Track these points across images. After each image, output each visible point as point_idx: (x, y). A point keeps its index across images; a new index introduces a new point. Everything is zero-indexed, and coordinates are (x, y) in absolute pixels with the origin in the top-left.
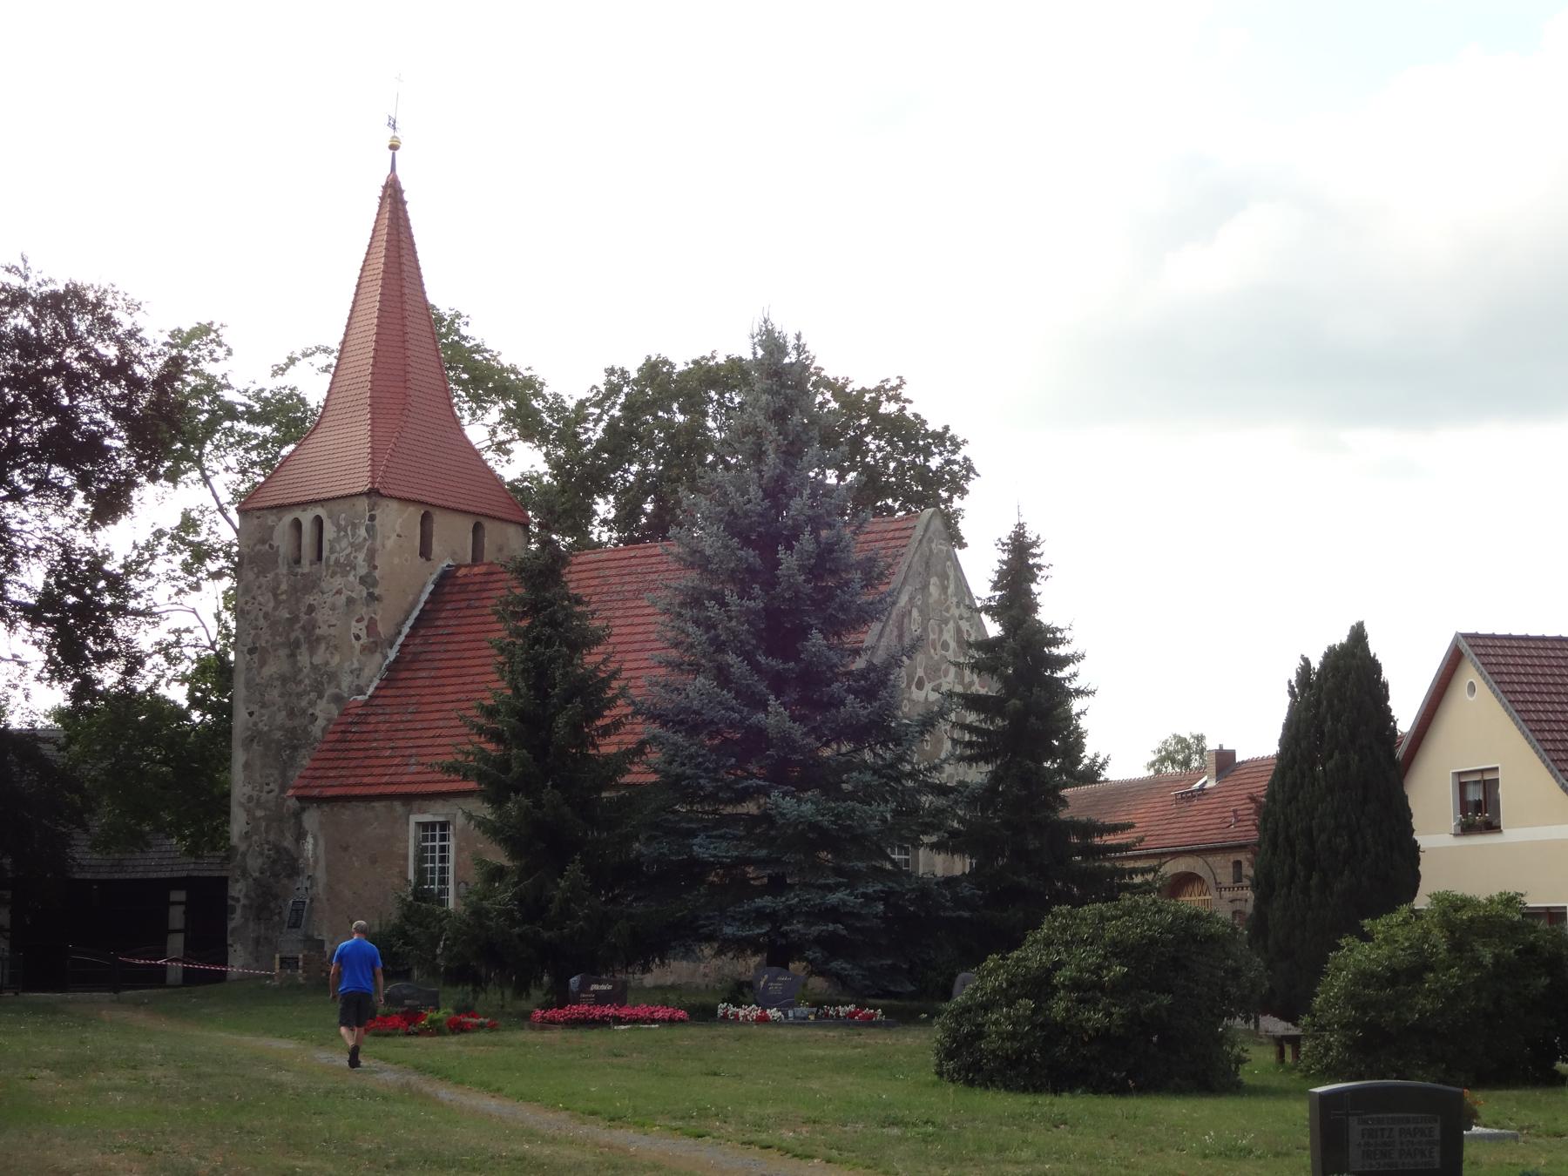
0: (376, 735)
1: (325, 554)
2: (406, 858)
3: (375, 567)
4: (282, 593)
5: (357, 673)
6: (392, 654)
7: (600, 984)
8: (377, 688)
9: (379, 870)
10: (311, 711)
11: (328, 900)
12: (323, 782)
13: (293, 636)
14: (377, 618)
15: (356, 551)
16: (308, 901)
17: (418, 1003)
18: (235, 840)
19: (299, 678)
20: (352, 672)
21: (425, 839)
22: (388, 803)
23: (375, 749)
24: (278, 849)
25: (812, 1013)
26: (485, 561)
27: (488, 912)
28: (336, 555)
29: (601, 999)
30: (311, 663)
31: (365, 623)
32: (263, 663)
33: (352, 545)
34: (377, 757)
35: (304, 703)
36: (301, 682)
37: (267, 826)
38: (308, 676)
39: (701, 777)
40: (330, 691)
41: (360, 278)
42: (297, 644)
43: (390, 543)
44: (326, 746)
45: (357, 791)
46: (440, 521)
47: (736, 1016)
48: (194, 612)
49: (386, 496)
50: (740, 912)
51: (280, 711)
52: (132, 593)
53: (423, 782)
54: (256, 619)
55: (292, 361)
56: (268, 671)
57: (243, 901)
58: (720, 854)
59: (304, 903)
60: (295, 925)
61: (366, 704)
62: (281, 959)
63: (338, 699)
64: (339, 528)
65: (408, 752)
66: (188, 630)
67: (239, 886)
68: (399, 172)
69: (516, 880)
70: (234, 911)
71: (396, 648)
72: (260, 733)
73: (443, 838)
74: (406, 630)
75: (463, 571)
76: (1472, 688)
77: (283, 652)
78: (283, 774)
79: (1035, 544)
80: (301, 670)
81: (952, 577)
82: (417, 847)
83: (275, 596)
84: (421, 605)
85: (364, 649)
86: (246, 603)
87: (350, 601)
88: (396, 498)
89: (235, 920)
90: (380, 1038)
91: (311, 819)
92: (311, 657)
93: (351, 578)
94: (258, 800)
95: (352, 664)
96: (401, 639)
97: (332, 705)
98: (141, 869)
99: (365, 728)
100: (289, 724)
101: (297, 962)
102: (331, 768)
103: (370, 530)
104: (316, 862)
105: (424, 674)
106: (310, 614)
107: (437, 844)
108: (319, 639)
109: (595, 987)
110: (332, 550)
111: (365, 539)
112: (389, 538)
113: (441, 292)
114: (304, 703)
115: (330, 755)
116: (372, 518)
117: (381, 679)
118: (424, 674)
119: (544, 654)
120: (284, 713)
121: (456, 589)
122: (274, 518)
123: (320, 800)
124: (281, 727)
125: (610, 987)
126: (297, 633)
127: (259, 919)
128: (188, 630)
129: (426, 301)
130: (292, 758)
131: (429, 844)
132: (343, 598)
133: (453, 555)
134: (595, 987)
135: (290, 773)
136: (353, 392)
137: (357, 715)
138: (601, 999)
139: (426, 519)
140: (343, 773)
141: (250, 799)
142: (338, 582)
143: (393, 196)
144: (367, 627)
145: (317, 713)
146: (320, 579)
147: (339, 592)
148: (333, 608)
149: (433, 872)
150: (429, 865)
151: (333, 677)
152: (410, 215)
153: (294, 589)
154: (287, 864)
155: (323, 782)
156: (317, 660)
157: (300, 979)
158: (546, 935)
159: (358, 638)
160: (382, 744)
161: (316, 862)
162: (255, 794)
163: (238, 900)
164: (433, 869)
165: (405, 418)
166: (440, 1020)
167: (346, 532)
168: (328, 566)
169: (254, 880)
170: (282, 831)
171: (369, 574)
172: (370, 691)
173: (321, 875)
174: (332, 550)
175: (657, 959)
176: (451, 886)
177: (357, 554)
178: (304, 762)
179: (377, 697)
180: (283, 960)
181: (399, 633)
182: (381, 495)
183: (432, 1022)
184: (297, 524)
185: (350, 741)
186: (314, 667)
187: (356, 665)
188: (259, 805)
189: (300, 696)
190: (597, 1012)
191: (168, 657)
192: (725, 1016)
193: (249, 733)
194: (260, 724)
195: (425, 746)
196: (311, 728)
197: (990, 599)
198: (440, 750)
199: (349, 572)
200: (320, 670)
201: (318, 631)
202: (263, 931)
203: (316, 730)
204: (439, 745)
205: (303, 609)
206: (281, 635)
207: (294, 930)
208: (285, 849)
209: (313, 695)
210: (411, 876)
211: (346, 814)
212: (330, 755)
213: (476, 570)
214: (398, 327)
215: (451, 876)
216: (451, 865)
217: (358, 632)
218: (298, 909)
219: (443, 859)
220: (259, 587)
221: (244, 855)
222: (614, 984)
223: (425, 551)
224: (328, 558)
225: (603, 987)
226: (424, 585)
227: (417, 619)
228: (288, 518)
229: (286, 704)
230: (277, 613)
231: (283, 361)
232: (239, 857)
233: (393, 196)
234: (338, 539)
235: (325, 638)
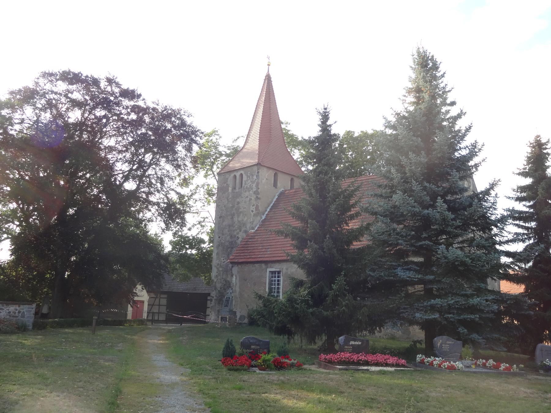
0: (257, 242)
1: (243, 185)
2: (266, 284)
3: (259, 188)
4: (230, 199)
5: (252, 223)
6: (264, 217)
7: (355, 341)
8: (258, 228)
9: (256, 288)
11: (239, 298)
14: (259, 205)
17: (258, 347)
18: (213, 278)
19: (234, 225)
21: (272, 277)
22: (260, 264)
23: (257, 246)
24: (226, 281)
25: (473, 364)
26: (295, 188)
27: (296, 300)
29: (356, 350)
30: (238, 220)
31: (255, 206)
33: (251, 182)
34: (257, 249)
35: (235, 233)
36: (235, 226)
39: (399, 240)
40: (243, 229)
41: (257, 103)
42: (234, 215)
43: (264, 181)
44: (241, 246)
45: (250, 260)
46: (280, 176)
47: (431, 364)
48: (208, 212)
49: (263, 166)
50: (421, 307)
51: (228, 236)
52: (186, 198)
53: (272, 257)
54: (222, 207)
55: (238, 138)
56: (224, 224)
57: (215, 298)
58: (412, 277)
59: (230, 298)
60: (226, 306)
61: (254, 233)
62: (221, 317)
63: (246, 232)
64: (248, 176)
65: (267, 247)
66: (207, 218)
68: (270, 72)
69: (309, 285)
71: (265, 215)
72: (222, 243)
73: (279, 277)
74: (268, 210)
75: (287, 192)
77: (229, 217)
79: (545, 144)
80: (235, 223)
81: (471, 183)
82: (269, 280)
83: (228, 200)
84: (273, 203)
85: (254, 215)
86: (219, 202)
88: (266, 167)
90: (231, 372)
91: (235, 270)
92: (238, 218)
93: (251, 192)
94: (220, 265)
96: (266, 213)
97: (244, 234)
98: (200, 290)
99: (253, 240)
100: (231, 240)
101: (226, 319)
102: (242, 253)
103: (258, 176)
104: (236, 284)
105: (273, 223)
107: (276, 279)
109: (352, 343)
110: (245, 184)
111: (256, 179)
112: (263, 179)
113: (283, 116)
115: (243, 249)
116: (258, 172)
117: (260, 225)
118: (273, 223)
119: (324, 178)
120: (229, 237)
121: (285, 197)
125: (360, 343)
128: (207, 218)
129: (280, 120)
130: (231, 251)
131: (274, 279)
134: (352, 343)
136: (254, 137)
137: (252, 236)
138: (356, 350)
139: (276, 175)
140: (246, 254)
141: (218, 264)
142: (247, 194)
143: (268, 79)
144: (255, 208)
145: (239, 236)
147: (247, 197)
149: (275, 289)
150: (273, 286)
151: (244, 224)
152: (273, 85)
154: (227, 285)
156: (240, 219)
157: (227, 325)
158: (325, 313)
159: (252, 211)
160: (258, 245)
161: (236, 284)
162: (219, 263)
163: (213, 297)
164: (275, 288)
165: (269, 145)
166: (269, 360)
167: (250, 178)
168: (244, 189)
171: (257, 191)
173: (238, 289)
174: (245, 184)
175: (378, 328)
176: (281, 294)
179: (258, 230)
180: (222, 318)
181: (266, 211)
182: (261, 165)
183: (264, 361)
185: (249, 244)
186: (239, 221)
187: (252, 221)
189: (234, 231)
190: (355, 357)
191: (202, 226)
192: (422, 362)
194: (222, 241)
195: (273, 245)
197: (524, 169)
198: (278, 246)
199: (250, 190)
201: (240, 210)
203: (239, 242)
204: (278, 245)
207: (226, 307)
208: (228, 281)
209: (238, 231)
210: (267, 290)
211: (247, 268)
212: (243, 249)
213: (291, 191)
215: (281, 290)
216: (281, 287)
217: (253, 210)
218: (228, 300)
219: (278, 284)
221: (215, 283)
222: (362, 341)
223: (275, 185)
224: (244, 186)
225: (357, 343)
226: (274, 196)
227: (272, 206)
228: (232, 175)
229: (229, 234)
231: (238, 139)
233: (268, 79)
234: (247, 180)
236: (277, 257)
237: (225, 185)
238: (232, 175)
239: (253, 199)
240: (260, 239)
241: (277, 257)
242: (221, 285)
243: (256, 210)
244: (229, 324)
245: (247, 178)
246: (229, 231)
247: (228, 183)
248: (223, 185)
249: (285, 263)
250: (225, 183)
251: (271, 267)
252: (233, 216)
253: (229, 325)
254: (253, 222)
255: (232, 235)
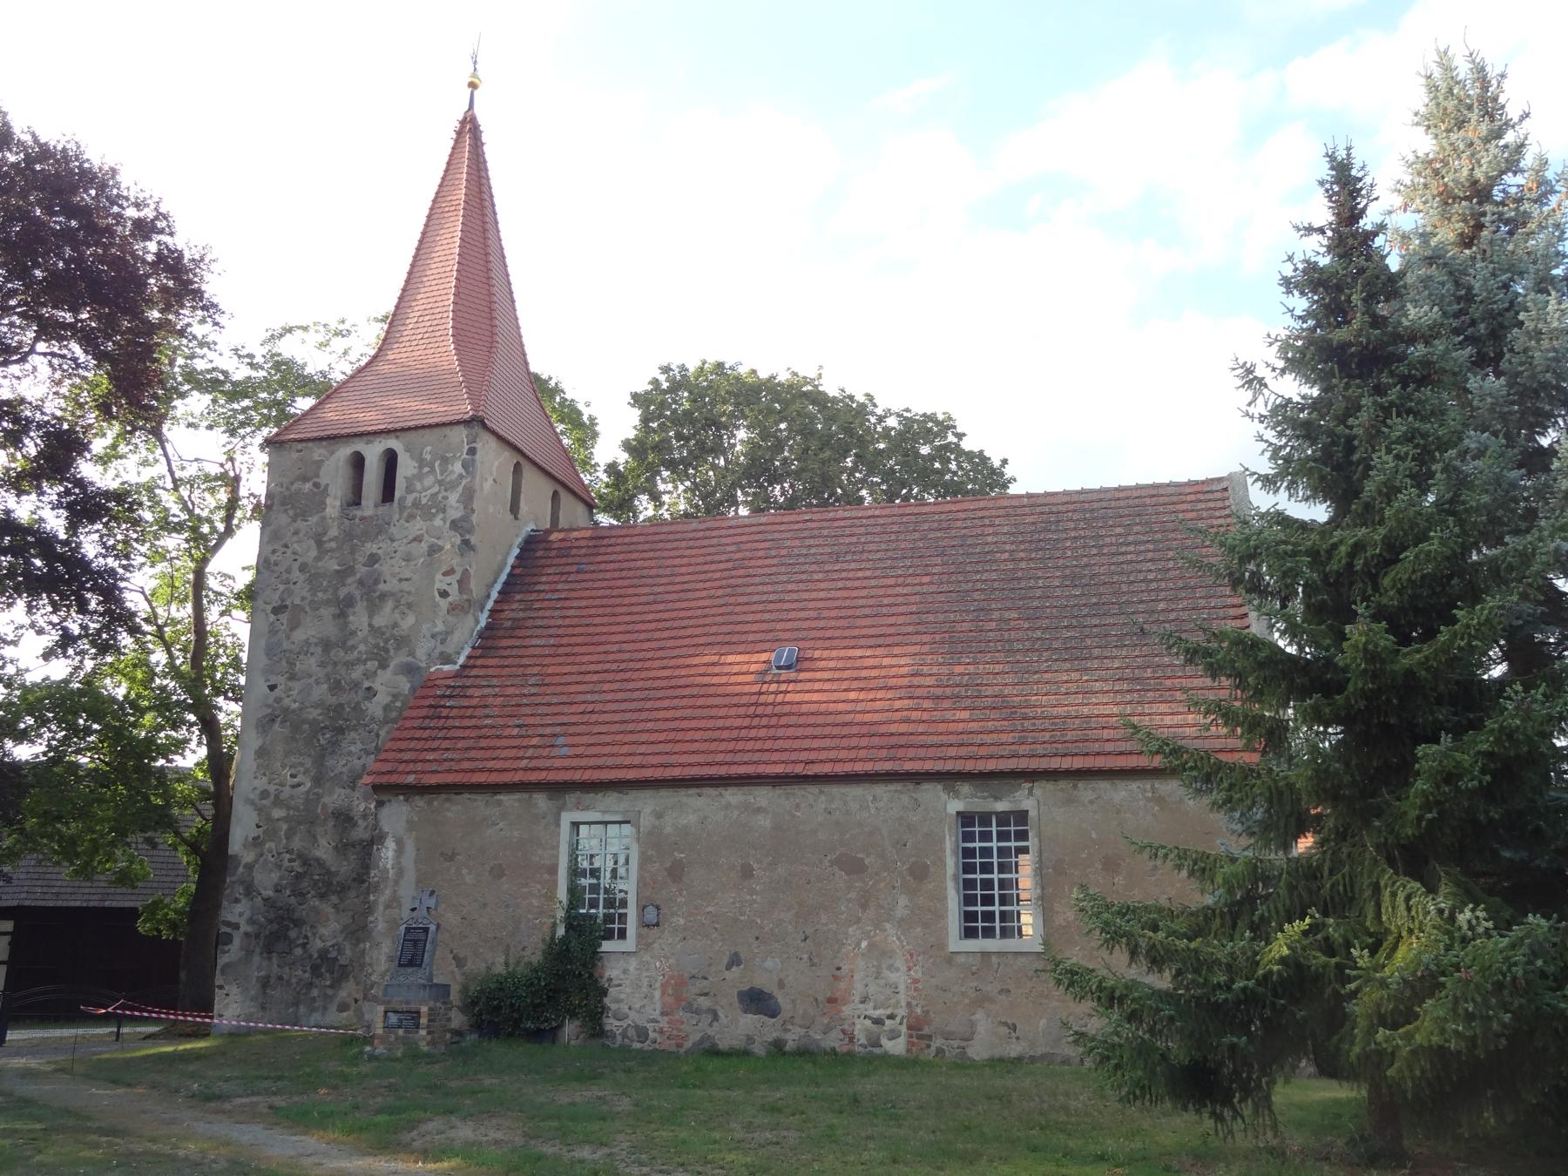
0: (487, 711)
1: (398, 494)
2: (553, 870)
4: (331, 540)
5: (443, 637)
10: (366, 684)
12: (419, 767)
13: (343, 593)
15: (446, 490)
16: (432, 928)
19: (350, 643)
20: (433, 636)
22: (526, 796)
28: (415, 495)
30: (370, 625)
31: (457, 576)
32: (294, 625)
33: (440, 483)
37: (290, 829)
38: (365, 641)
41: (431, 209)
42: (349, 602)
43: (488, 485)
45: (1100, 763)
54: (288, 571)
55: (290, 330)
56: (299, 635)
57: (244, 928)
59: (426, 930)
61: (457, 675)
63: (409, 670)
64: (422, 463)
67: (239, 908)
68: (477, 111)
70: (229, 939)
71: (486, 614)
72: (286, 711)
74: (494, 595)
76: (124, 878)
77: (327, 612)
78: (320, 761)
80: (353, 633)
83: (319, 543)
84: (508, 570)
85: (453, 609)
87: (434, 550)
89: (230, 954)
91: (396, 816)
92: (370, 617)
93: (438, 522)
95: (436, 626)
96: (490, 605)
99: (465, 703)
100: (332, 700)
104: (400, 872)
106: (372, 566)
108: (383, 596)
111: (461, 476)
114: (356, 674)
116: (472, 451)
117: (473, 648)
120: (325, 686)
122: (322, 451)
123: (410, 791)
124: (320, 704)
126: (350, 588)
127: (270, 952)
130: (334, 744)
132: (424, 546)
133: (536, 520)
135: (330, 762)
137: (448, 687)
141: (264, 794)
142: (418, 526)
143: (469, 129)
145: (377, 686)
146: (389, 524)
147: (418, 539)
148: (408, 559)
151: (403, 642)
153: (348, 535)
155: (419, 767)
156: (379, 621)
159: (444, 594)
161: (400, 872)
162: (272, 788)
163: (236, 926)
168: (402, 508)
169: (266, 900)
170: (314, 837)
171: (465, 518)
172: (461, 660)
174: (409, 489)
177: (448, 494)
178: (353, 748)
181: (488, 596)
182: (485, 426)
184: (358, 462)
187: (440, 627)
188: (278, 802)
189: (350, 665)
193: (270, 711)
196: (365, 705)
199: (434, 515)
200: (383, 634)
201: (381, 586)
202: (275, 969)
203: (375, 708)
205: (361, 558)
206: (325, 591)
207: (410, 970)
208: (317, 860)
210: (562, 894)
211: (455, 810)
214: (482, 262)
220: (296, 533)
223: (514, 508)
224: (403, 499)
226: (510, 547)
228: (344, 452)
230: (320, 564)
232: (241, 869)
233: (469, 129)
234: (420, 477)
235: (392, 594)
236: (617, 767)
237: (308, 486)
238: (344, 452)
239: (448, 546)
240: (499, 701)
241: (617, 767)
242: (281, 878)
243: (461, 591)
244: (429, 1038)
245: (421, 467)
246: (322, 665)
247: (323, 481)
248: (294, 487)
249: (649, 793)
250: (305, 479)
251: (578, 806)
252: (344, 608)
253: (432, 1043)
254: (449, 633)
255: (338, 682)
